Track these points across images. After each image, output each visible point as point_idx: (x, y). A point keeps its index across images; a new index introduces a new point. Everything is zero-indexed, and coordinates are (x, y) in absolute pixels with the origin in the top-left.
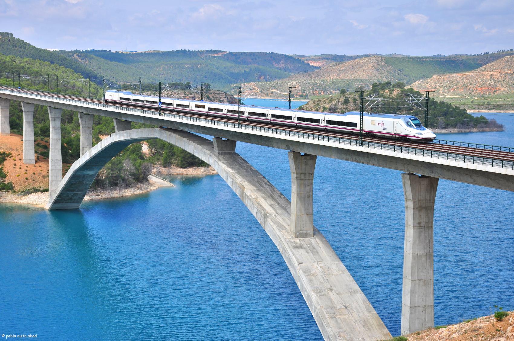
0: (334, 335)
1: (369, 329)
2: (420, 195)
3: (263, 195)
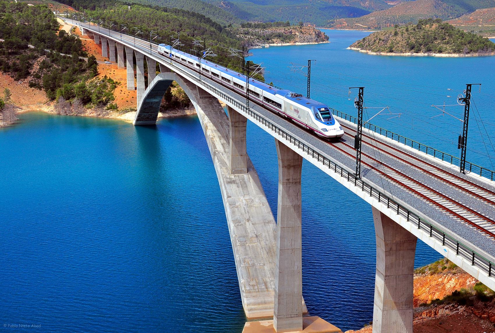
0: (240, 261)
1: (272, 256)
2: (289, 156)
3: (220, 134)
